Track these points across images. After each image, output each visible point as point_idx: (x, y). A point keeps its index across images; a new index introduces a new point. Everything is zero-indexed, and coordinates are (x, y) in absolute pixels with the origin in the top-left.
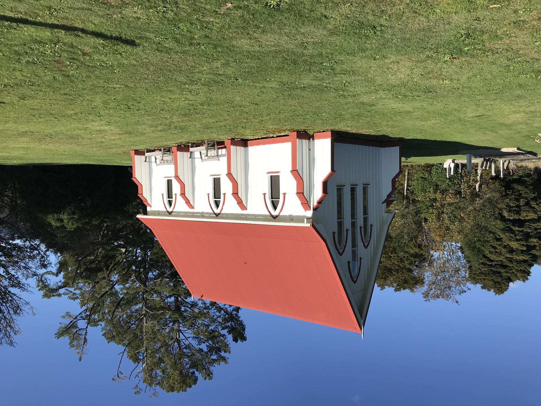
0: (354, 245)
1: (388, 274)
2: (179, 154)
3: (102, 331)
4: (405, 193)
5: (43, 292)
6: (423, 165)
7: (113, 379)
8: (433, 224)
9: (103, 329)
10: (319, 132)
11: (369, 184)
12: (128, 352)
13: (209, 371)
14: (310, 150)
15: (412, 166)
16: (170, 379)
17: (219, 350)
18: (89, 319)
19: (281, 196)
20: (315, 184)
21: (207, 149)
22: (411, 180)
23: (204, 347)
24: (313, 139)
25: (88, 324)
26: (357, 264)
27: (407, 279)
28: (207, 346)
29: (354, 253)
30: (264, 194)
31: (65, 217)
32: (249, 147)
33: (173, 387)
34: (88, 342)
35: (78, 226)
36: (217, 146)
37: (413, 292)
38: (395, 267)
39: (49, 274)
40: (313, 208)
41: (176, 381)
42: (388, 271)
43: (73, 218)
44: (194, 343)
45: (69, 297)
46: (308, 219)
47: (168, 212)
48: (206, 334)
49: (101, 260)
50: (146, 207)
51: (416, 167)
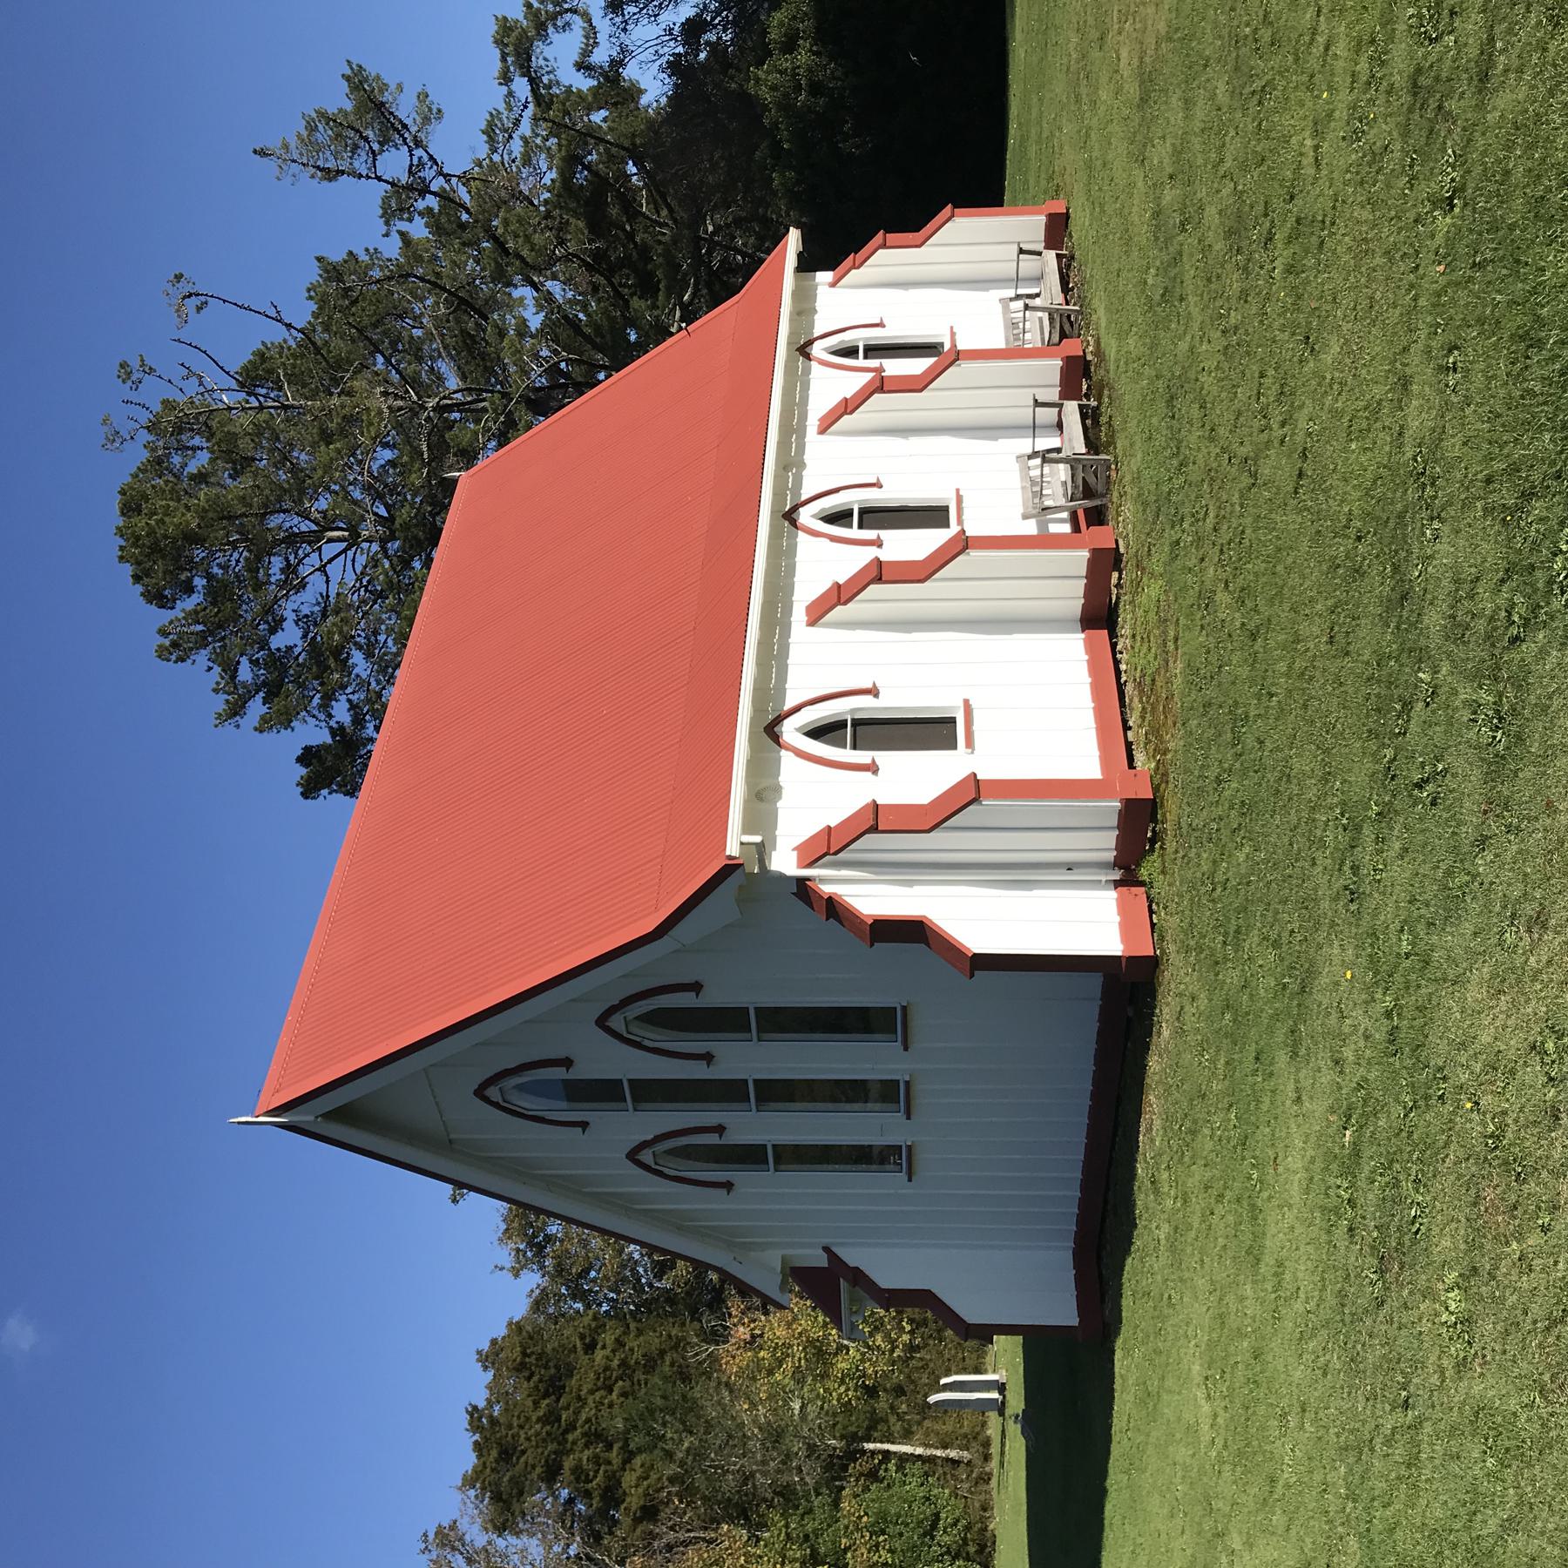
0: (648, 1092)
1: (540, 1381)
2: (1052, 367)
3: (367, 250)
4: (870, 1446)
5: (521, 17)
6: (991, 1527)
7: (182, 276)
8: (738, 1558)
9: (374, 253)
10: (1150, 907)
11: (910, 1180)
12: (282, 347)
13: (191, 649)
14: (1067, 871)
15: (986, 1478)
16: (172, 499)
17: (272, 691)
18: (409, 188)
19: (863, 757)
20: (915, 887)
21: (1073, 462)
22: (927, 1474)
23: (289, 637)
24: (1117, 884)
25: (393, 184)
26: (561, 1110)
27: (518, 1459)
28: (290, 649)
29: (605, 1092)
30: (873, 692)
31: (803, 57)
32: (1083, 636)
33: (139, 511)
34: (325, 183)
35: (766, 108)
36: (1086, 510)
37: (463, 1485)
38: (567, 1408)
39: (587, 37)
40: (808, 879)
41: (162, 519)
42: (552, 1378)
43: (798, 88)
44: (306, 601)
45: (499, 113)
46: (762, 851)
47: (810, 343)
48: (336, 637)
49: (635, 243)
50: (832, 268)
51: (982, 1497)
